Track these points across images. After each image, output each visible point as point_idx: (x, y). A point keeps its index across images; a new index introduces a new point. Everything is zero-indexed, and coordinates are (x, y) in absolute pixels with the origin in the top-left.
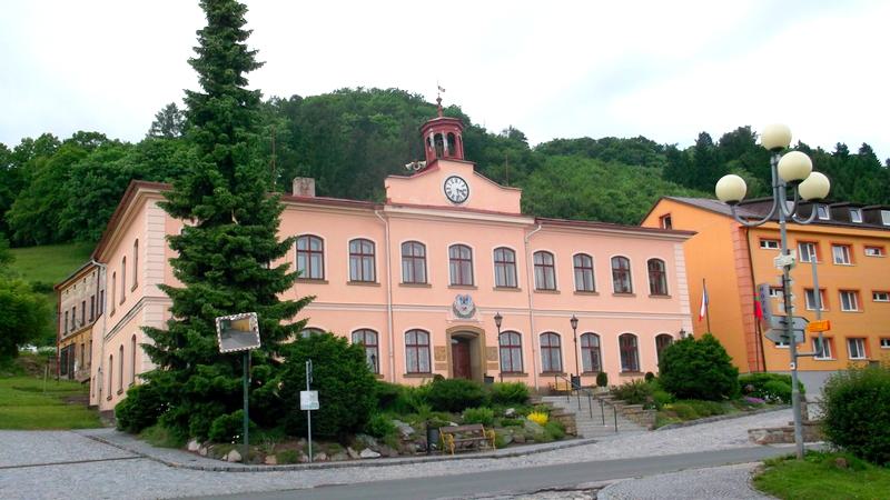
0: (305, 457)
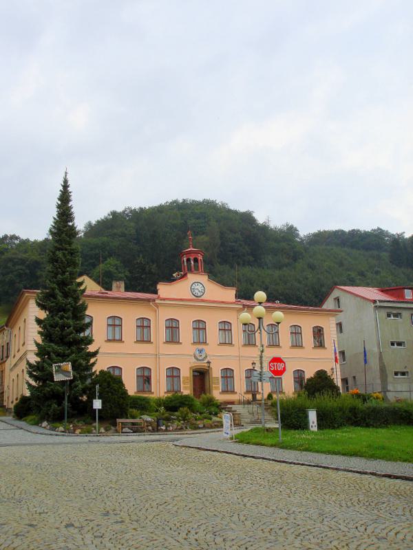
0: (94, 431)
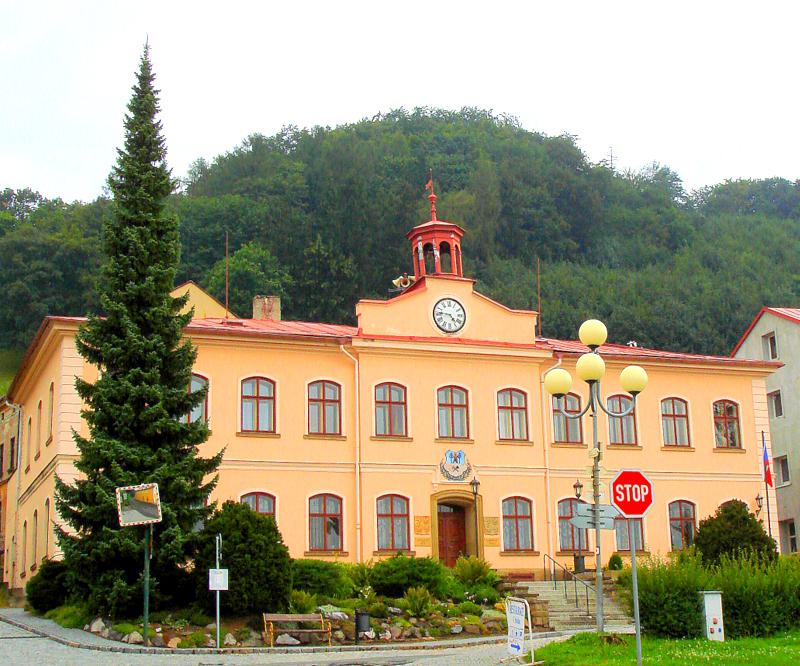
0: (212, 642)
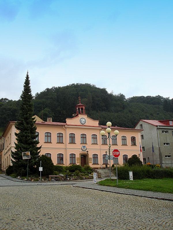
0: (40, 180)
